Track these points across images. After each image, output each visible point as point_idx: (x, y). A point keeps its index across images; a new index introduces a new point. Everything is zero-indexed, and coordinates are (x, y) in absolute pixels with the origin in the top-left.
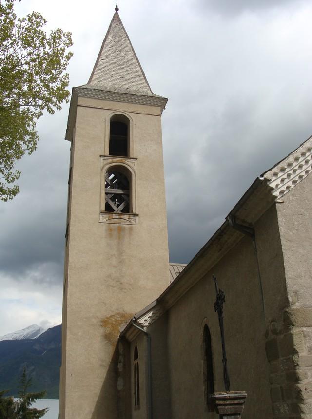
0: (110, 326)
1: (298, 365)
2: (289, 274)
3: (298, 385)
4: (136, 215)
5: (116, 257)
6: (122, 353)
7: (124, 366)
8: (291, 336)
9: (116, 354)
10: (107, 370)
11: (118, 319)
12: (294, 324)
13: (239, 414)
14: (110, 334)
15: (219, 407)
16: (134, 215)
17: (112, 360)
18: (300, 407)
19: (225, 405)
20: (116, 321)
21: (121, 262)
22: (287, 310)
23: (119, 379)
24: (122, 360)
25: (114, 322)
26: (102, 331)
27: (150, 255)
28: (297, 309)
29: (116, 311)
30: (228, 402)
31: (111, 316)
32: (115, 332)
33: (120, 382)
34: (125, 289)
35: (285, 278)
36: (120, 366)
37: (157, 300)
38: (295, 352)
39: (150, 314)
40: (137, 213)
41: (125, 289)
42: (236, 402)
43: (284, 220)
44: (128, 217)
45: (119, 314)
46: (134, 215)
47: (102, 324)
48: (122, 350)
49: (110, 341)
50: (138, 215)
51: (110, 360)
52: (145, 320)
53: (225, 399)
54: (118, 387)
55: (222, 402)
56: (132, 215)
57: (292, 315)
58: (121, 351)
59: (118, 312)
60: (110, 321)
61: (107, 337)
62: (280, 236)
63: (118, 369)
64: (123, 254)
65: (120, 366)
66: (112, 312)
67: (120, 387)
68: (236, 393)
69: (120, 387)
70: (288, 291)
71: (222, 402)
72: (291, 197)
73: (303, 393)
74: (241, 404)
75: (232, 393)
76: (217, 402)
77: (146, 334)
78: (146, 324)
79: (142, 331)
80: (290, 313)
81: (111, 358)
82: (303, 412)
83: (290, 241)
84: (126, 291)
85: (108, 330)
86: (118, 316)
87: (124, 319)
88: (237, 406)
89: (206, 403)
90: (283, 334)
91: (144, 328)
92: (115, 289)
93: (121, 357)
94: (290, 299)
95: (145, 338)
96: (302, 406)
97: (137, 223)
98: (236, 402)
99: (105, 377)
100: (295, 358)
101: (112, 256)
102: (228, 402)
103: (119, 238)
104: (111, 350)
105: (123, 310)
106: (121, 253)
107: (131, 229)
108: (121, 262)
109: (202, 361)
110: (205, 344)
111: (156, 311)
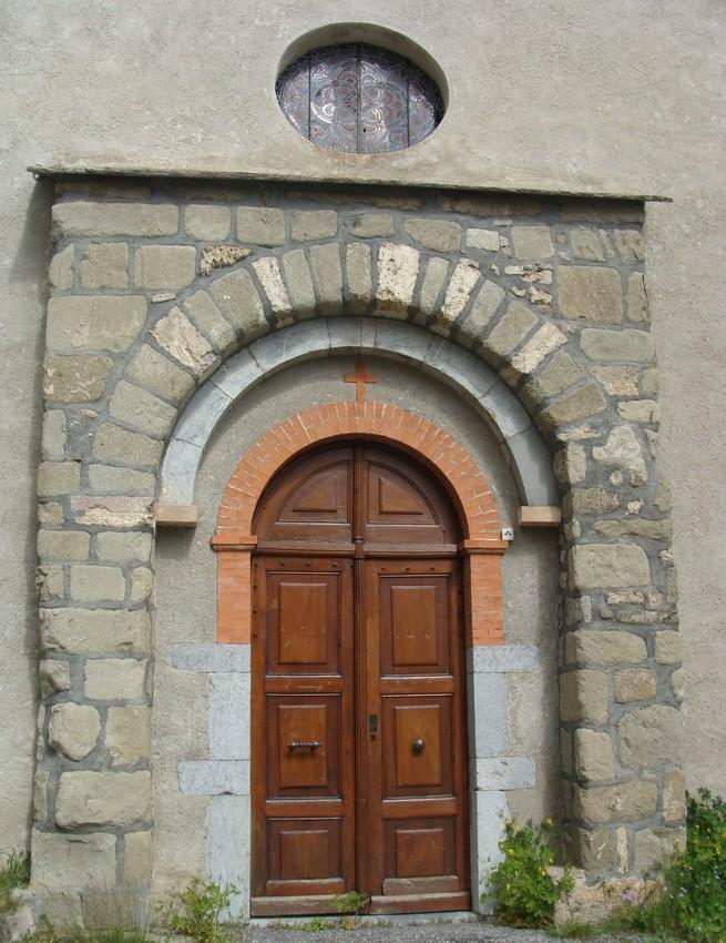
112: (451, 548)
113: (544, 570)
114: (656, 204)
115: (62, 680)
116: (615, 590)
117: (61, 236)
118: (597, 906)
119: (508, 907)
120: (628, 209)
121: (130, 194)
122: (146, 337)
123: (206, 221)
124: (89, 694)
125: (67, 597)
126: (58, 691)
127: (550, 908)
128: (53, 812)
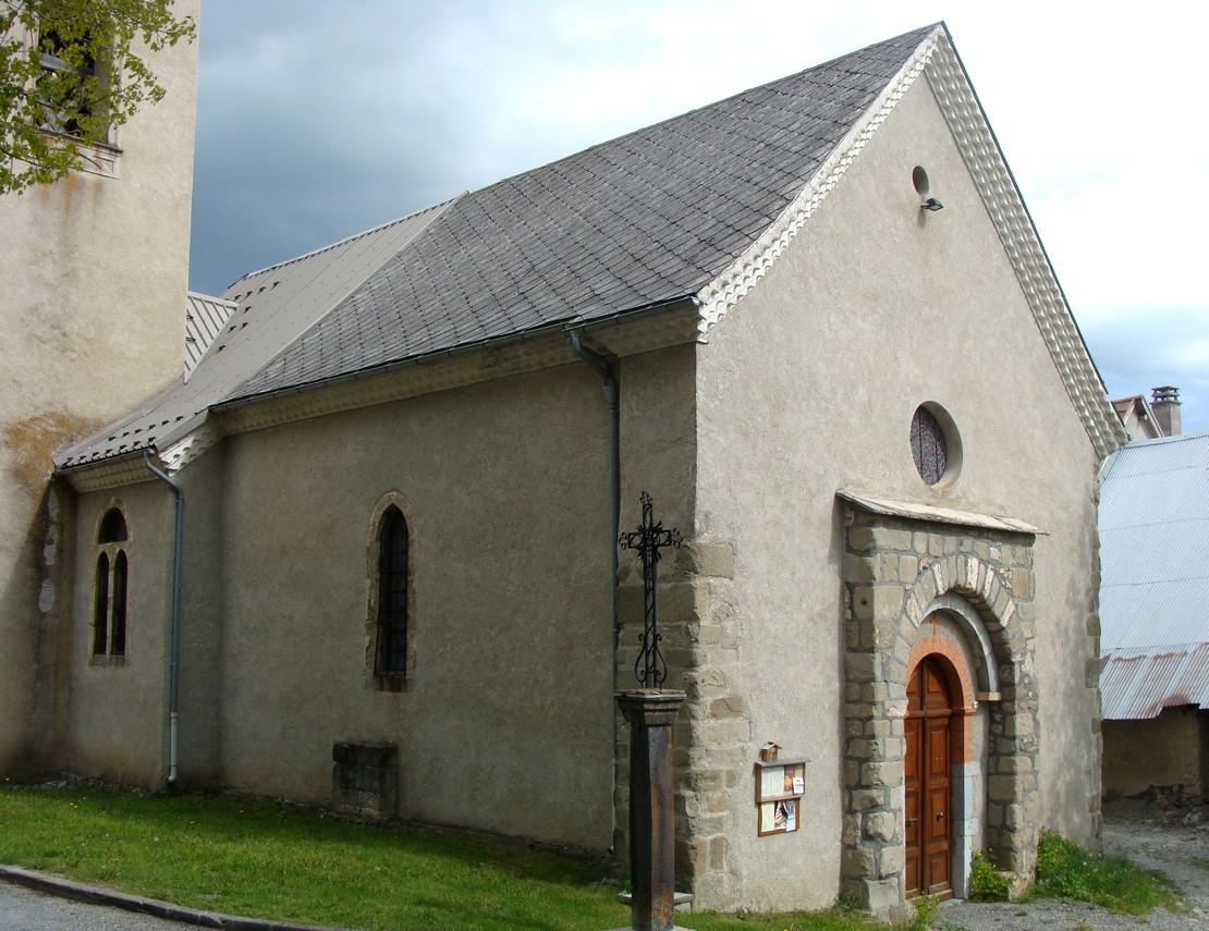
0: (28, 446)
1: (697, 641)
2: (702, 481)
3: (693, 674)
4: (116, 151)
5: (54, 262)
6: (56, 520)
7: (60, 550)
8: (691, 590)
9: (42, 516)
10: (15, 561)
11: (50, 429)
12: (699, 570)
13: (669, 725)
14: (27, 466)
15: (646, 714)
16: (111, 150)
17: (30, 534)
18: (690, 711)
19: (655, 711)
20: (46, 433)
21: (69, 276)
22: (689, 544)
23: (44, 585)
24: (56, 537)
25: (39, 437)
26: (8, 456)
27: (143, 268)
28: (706, 546)
29: (48, 409)
30: (659, 707)
31: (33, 419)
32: (40, 464)
33: (48, 592)
34: (73, 351)
35: (695, 488)
36: (50, 552)
37: (211, 408)
38: (695, 618)
39: (188, 443)
40: (120, 146)
41: (73, 351)
42: (670, 706)
43: (705, 379)
44: (93, 153)
45: (52, 415)
46: (111, 150)
47: (7, 438)
48: (56, 511)
49: (26, 484)
50: (121, 152)
51: (25, 535)
52: (177, 456)
53: (656, 702)
54: (41, 604)
55: (652, 707)
56: (107, 148)
57: (696, 554)
58: (54, 514)
59: (52, 410)
60: (29, 432)
61: (20, 474)
62: (694, 409)
63: (44, 559)
64: (76, 255)
65: (50, 552)
66: (37, 408)
67: (46, 605)
68: (673, 693)
69: (46, 605)
70: (697, 512)
71: (652, 707)
72: (718, 335)
73: (699, 687)
74: (674, 710)
75: (667, 693)
76: (646, 706)
77: (175, 490)
78: (176, 465)
79: (161, 478)
80: (693, 551)
81: (27, 530)
82: (694, 717)
83: (710, 420)
84: (74, 356)
85: (25, 454)
86: (52, 422)
87: (65, 430)
88: (670, 713)
89: (371, 671)
90: (669, 582)
91: (171, 475)
92: (47, 347)
93: (52, 529)
94: (697, 526)
95: (170, 499)
96: (694, 707)
97: (117, 173)
98: (670, 706)
99: (8, 577)
100: (693, 627)
101: (44, 255)
102: (659, 707)
103: (67, 208)
104: (30, 507)
105: (66, 407)
106: (68, 250)
107: (99, 188)
108: (67, 275)
109: (368, 582)
110: (379, 545)
111: (204, 434)
112: (947, 711)
113: (985, 722)
114: (902, 537)
115: (880, 801)
116: (1025, 736)
117: (875, 548)
118: (782, 809)
119: (712, 798)
120: (1026, 538)
121: (948, 521)
122: (904, 611)
123: (921, 539)
124: (892, 806)
125: (884, 756)
126: (877, 806)
127: (1005, 890)
128: (878, 870)
